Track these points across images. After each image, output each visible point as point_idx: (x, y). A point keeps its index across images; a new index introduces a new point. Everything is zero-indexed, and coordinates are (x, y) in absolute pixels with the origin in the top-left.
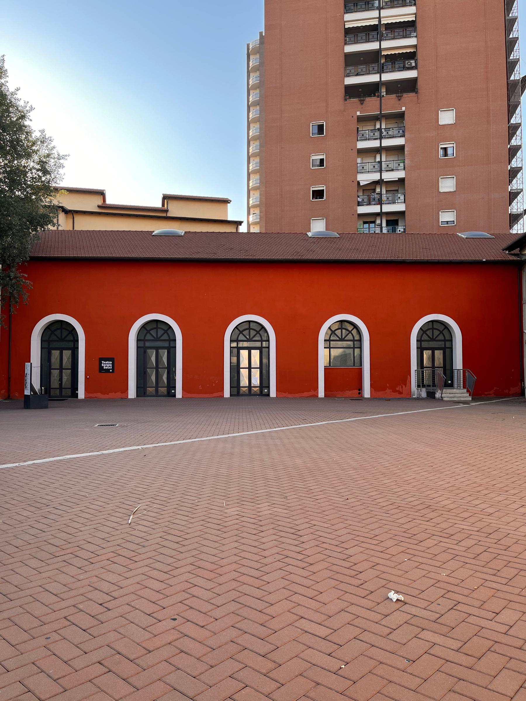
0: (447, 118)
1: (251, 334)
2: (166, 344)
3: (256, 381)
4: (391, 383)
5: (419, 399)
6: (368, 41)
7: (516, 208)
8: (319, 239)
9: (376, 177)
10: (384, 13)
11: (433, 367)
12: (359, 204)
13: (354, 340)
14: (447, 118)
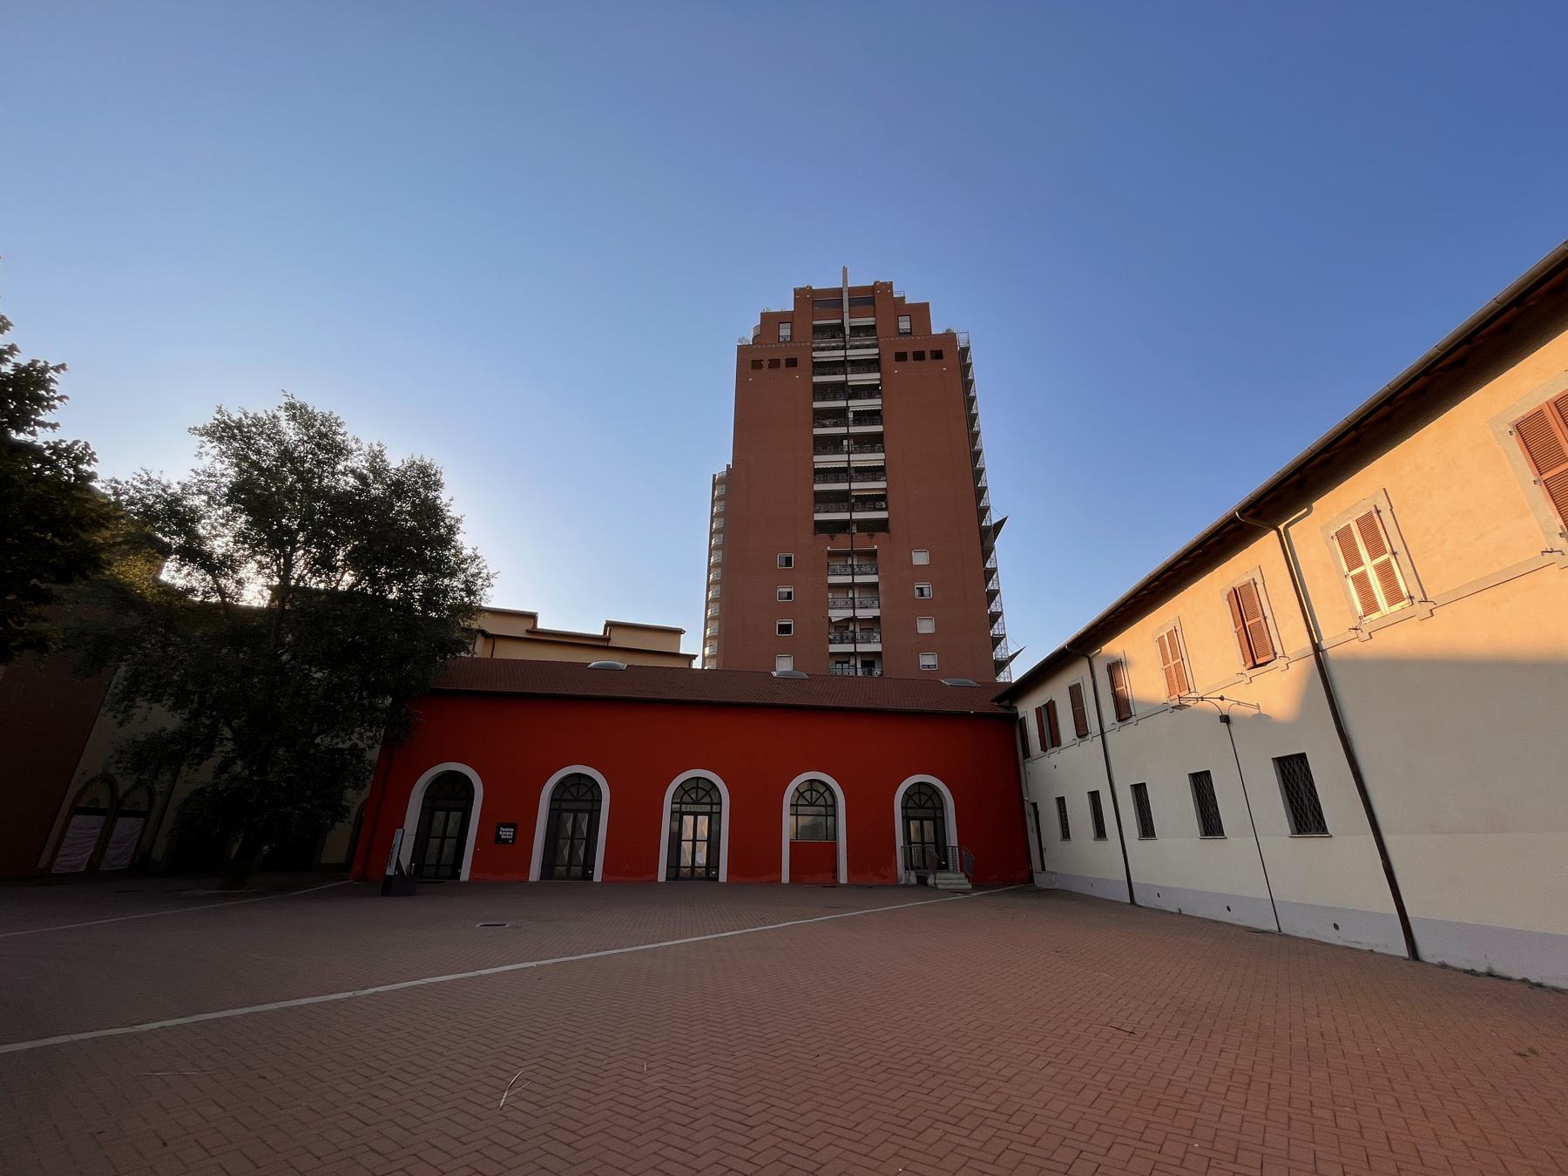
0: (920, 559)
1: (699, 794)
2: (588, 806)
3: (701, 859)
4: (872, 864)
5: (907, 886)
6: (838, 481)
7: (999, 654)
8: (784, 679)
9: (849, 613)
10: (853, 457)
11: (923, 842)
12: (831, 642)
13: (826, 806)
14: (920, 559)
